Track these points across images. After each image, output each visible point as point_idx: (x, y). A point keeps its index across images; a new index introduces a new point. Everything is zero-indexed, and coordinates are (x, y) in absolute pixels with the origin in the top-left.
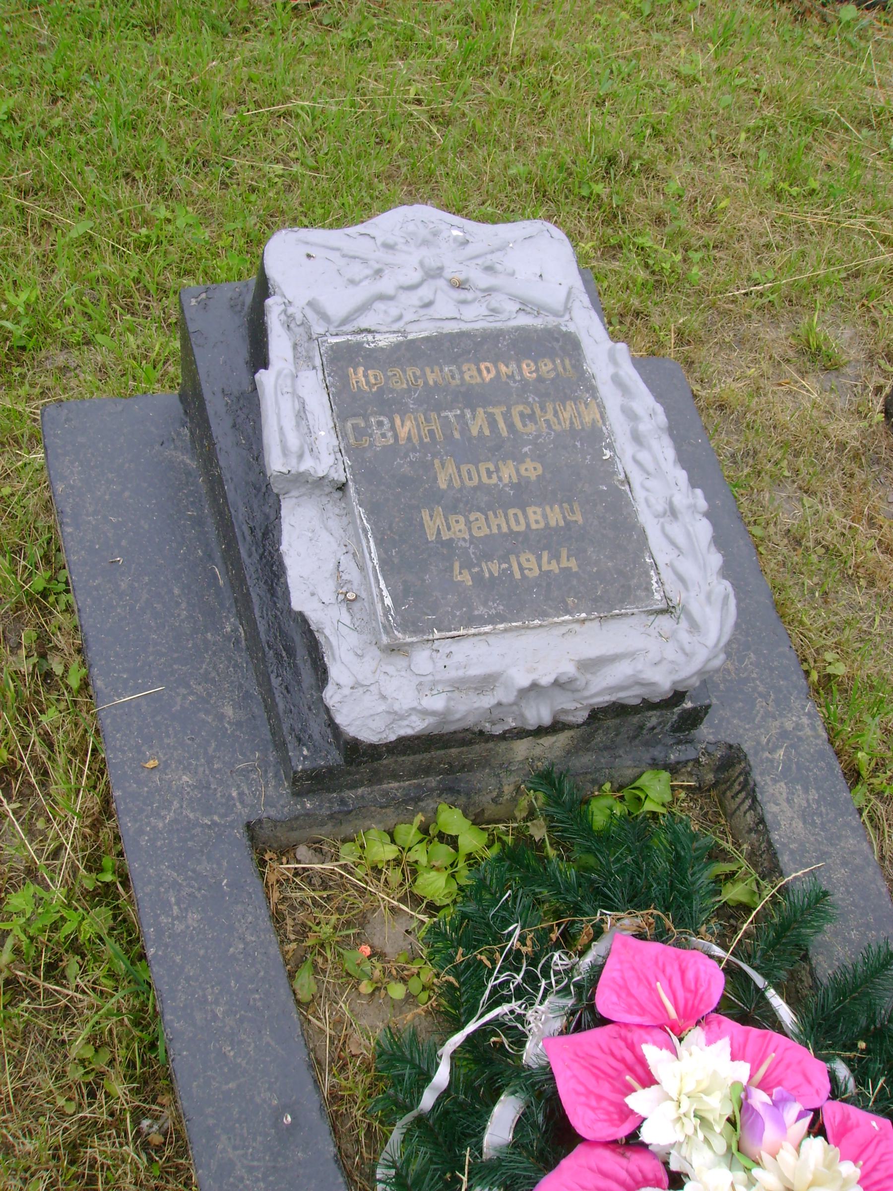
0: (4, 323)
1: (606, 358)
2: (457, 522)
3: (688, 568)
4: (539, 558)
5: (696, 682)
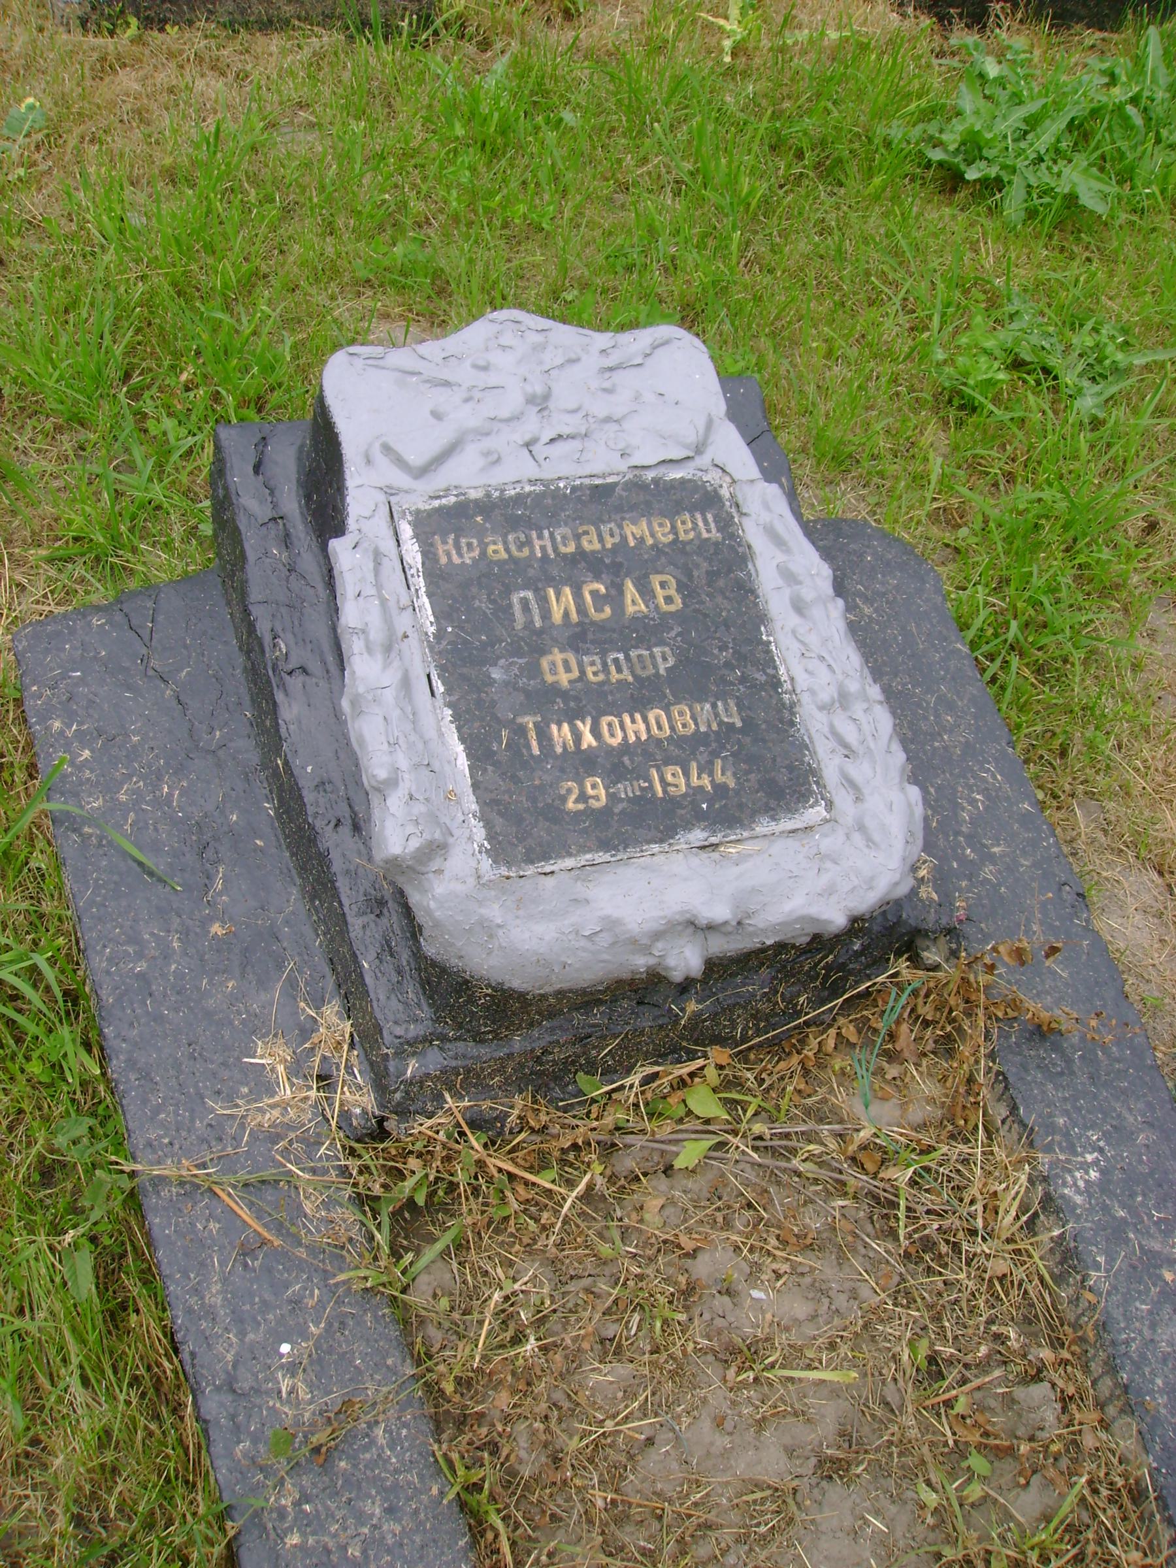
1: (766, 517)
2: (684, 726)
3: (860, 771)
4: (687, 774)
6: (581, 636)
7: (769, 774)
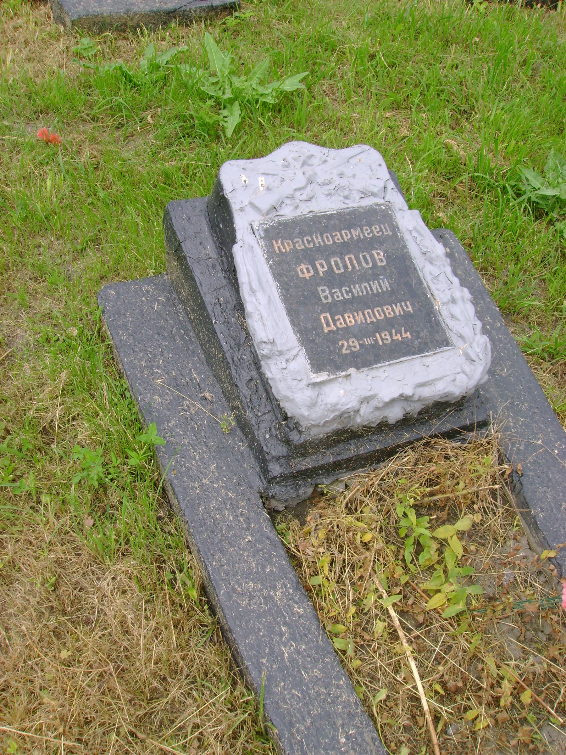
0: (447, 2)
1: (409, 222)
2: (350, 322)
5: (472, 391)
6: (332, 280)
7: (426, 333)
